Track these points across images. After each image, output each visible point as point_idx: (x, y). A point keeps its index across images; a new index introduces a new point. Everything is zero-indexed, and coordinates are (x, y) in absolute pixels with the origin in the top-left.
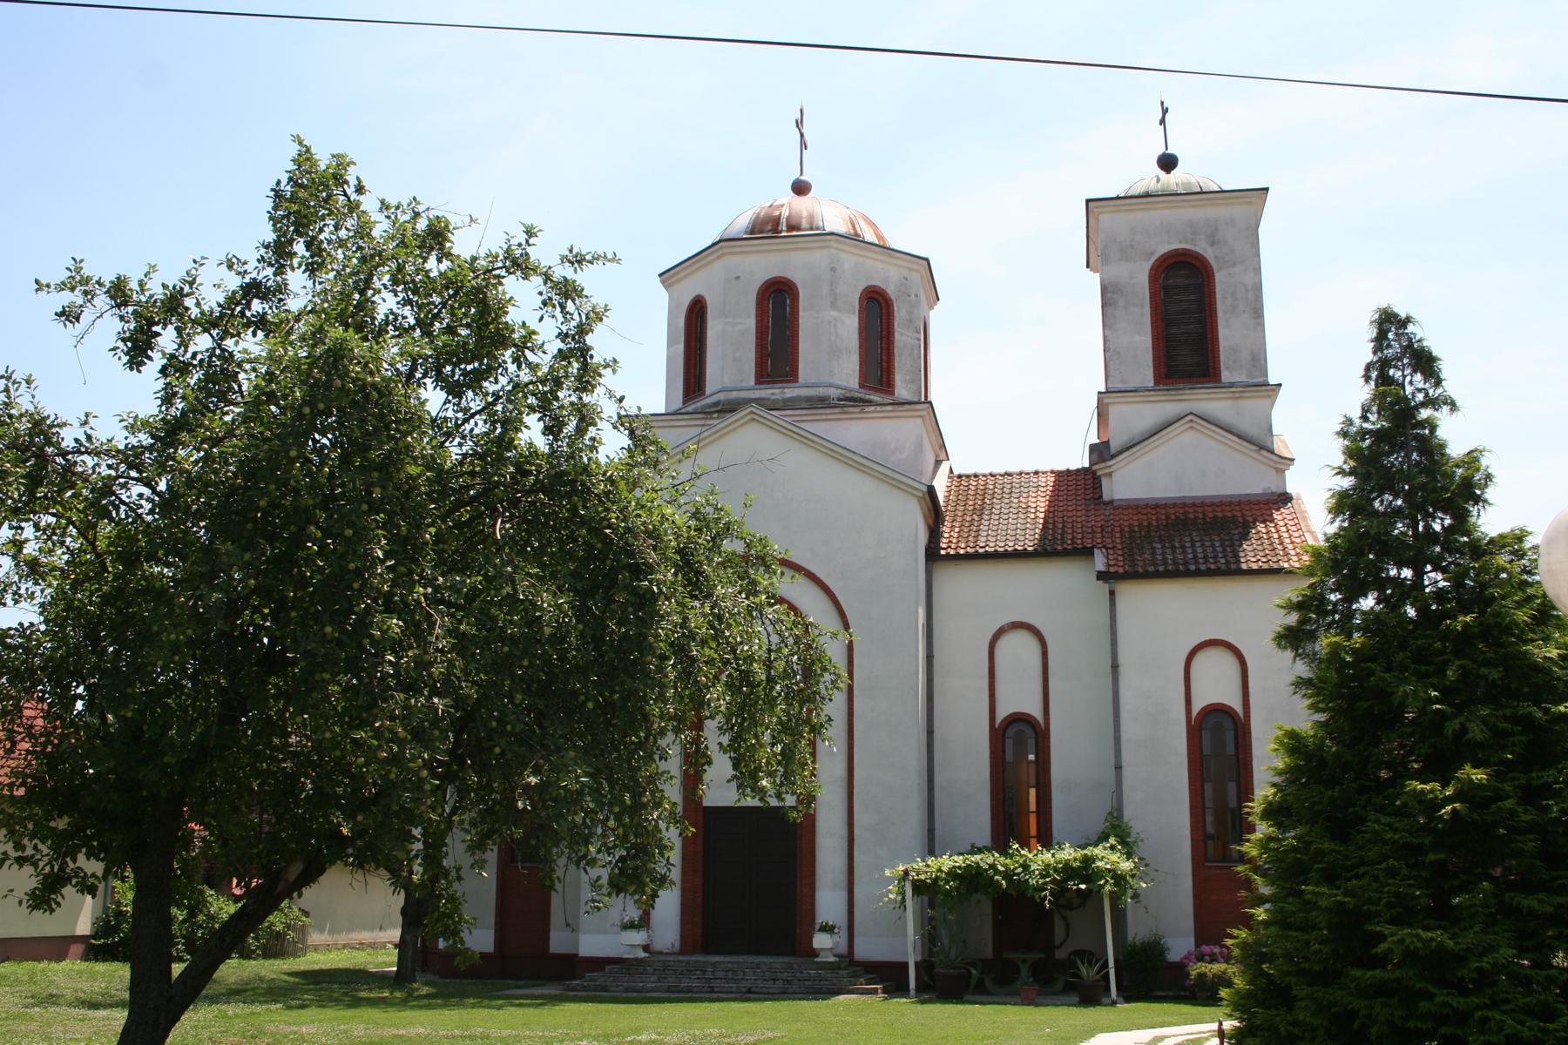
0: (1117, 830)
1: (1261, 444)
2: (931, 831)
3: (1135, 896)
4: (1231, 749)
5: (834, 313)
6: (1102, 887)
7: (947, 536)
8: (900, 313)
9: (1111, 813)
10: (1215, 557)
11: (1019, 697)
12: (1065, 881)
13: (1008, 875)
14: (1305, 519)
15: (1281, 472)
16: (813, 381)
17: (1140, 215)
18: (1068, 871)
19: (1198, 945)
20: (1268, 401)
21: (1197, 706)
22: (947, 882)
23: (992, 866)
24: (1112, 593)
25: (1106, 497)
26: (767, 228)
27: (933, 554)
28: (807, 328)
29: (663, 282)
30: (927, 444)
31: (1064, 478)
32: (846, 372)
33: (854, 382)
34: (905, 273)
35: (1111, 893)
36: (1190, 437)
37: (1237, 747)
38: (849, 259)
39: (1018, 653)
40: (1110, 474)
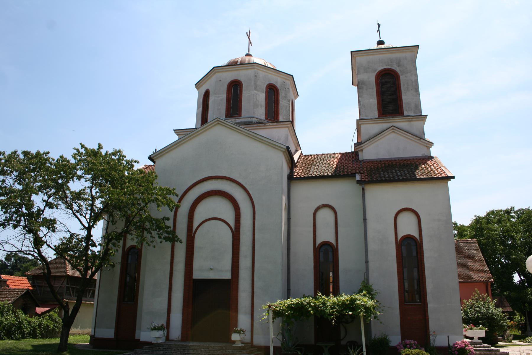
0: (366, 288)
1: (420, 137)
2: (289, 290)
3: (375, 317)
4: (414, 254)
5: (256, 92)
6: (359, 313)
7: (298, 172)
8: (282, 94)
9: (364, 281)
10: (406, 175)
11: (326, 235)
12: (343, 310)
13: (315, 308)
14: (440, 163)
15: (429, 148)
16: (247, 116)
17: (371, 57)
18: (344, 306)
19: (403, 338)
20: (422, 122)
21: (400, 236)
22: (287, 311)
23: (309, 303)
24: (363, 189)
25: (361, 159)
26: (233, 64)
27: (291, 178)
28: (246, 99)
29: (196, 87)
30: (290, 138)
31: (344, 156)
32: (261, 113)
33: (263, 117)
34: (284, 80)
35: (364, 316)
36: (393, 135)
37: (417, 253)
38: (262, 74)
39: (325, 216)
40: (362, 150)
